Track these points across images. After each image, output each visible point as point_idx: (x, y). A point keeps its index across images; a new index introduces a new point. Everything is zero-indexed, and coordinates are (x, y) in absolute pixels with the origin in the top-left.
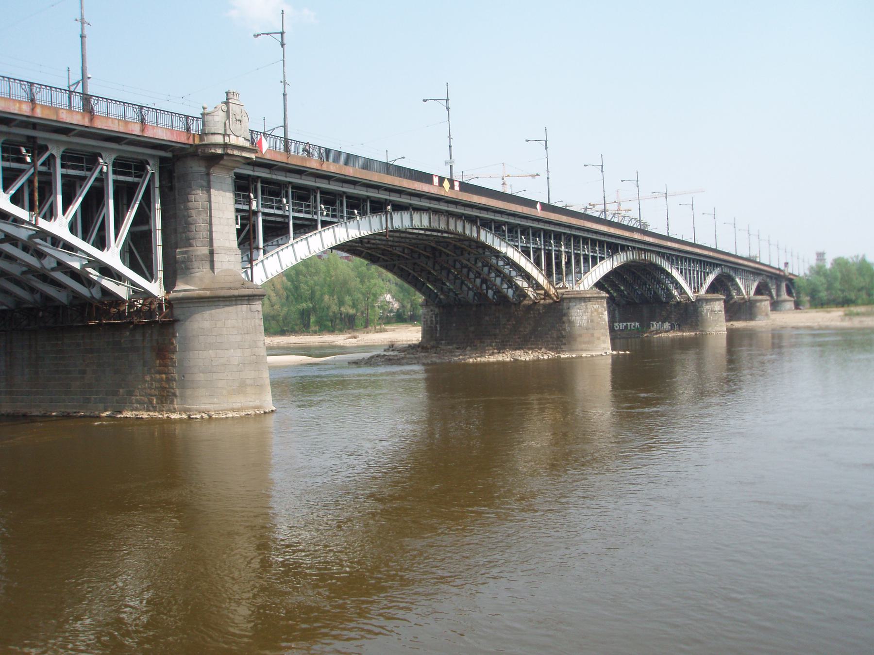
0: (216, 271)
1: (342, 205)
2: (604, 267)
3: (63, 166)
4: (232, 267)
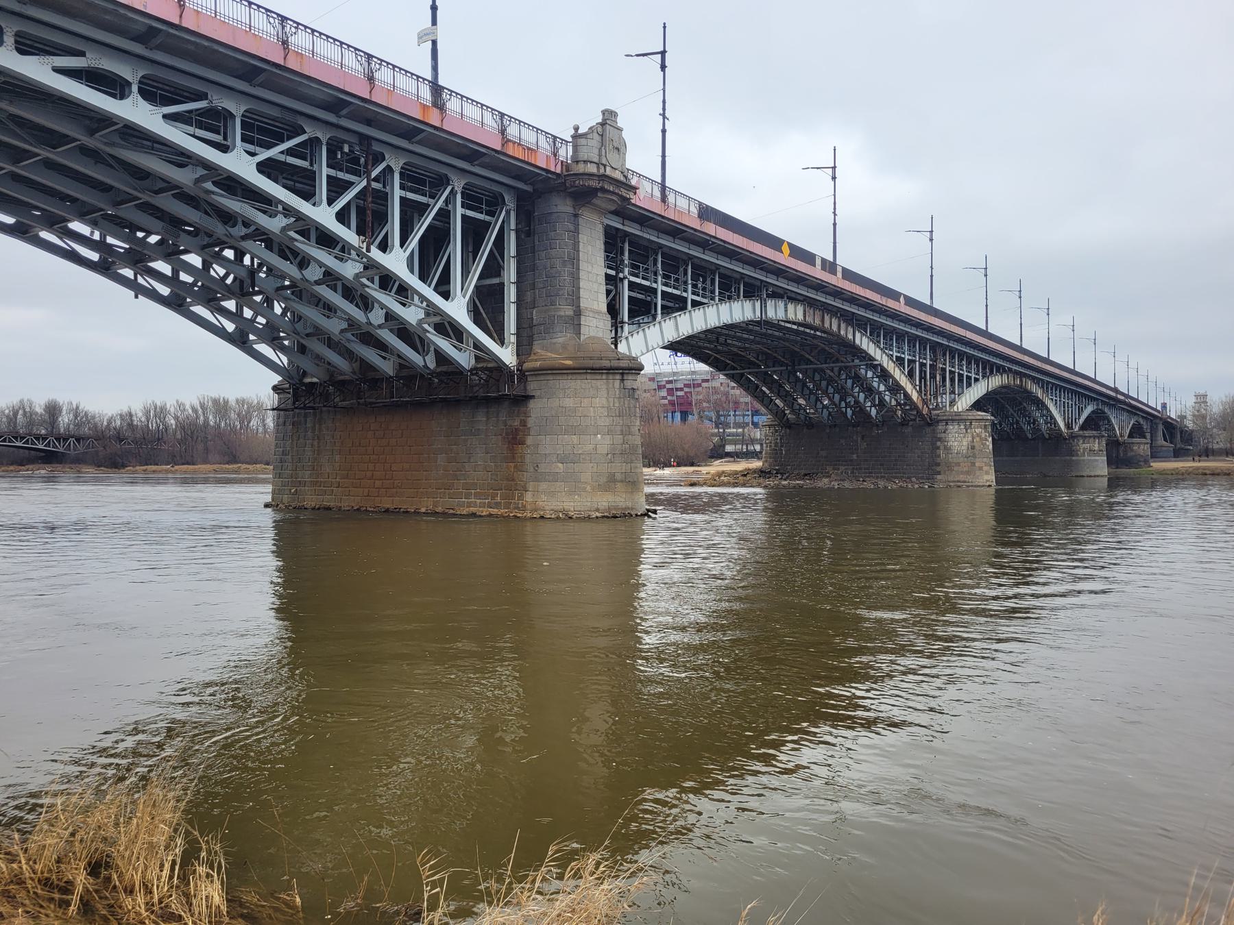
0: (582, 338)
2: (978, 390)
3: (402, 187)
4: (600, 335)
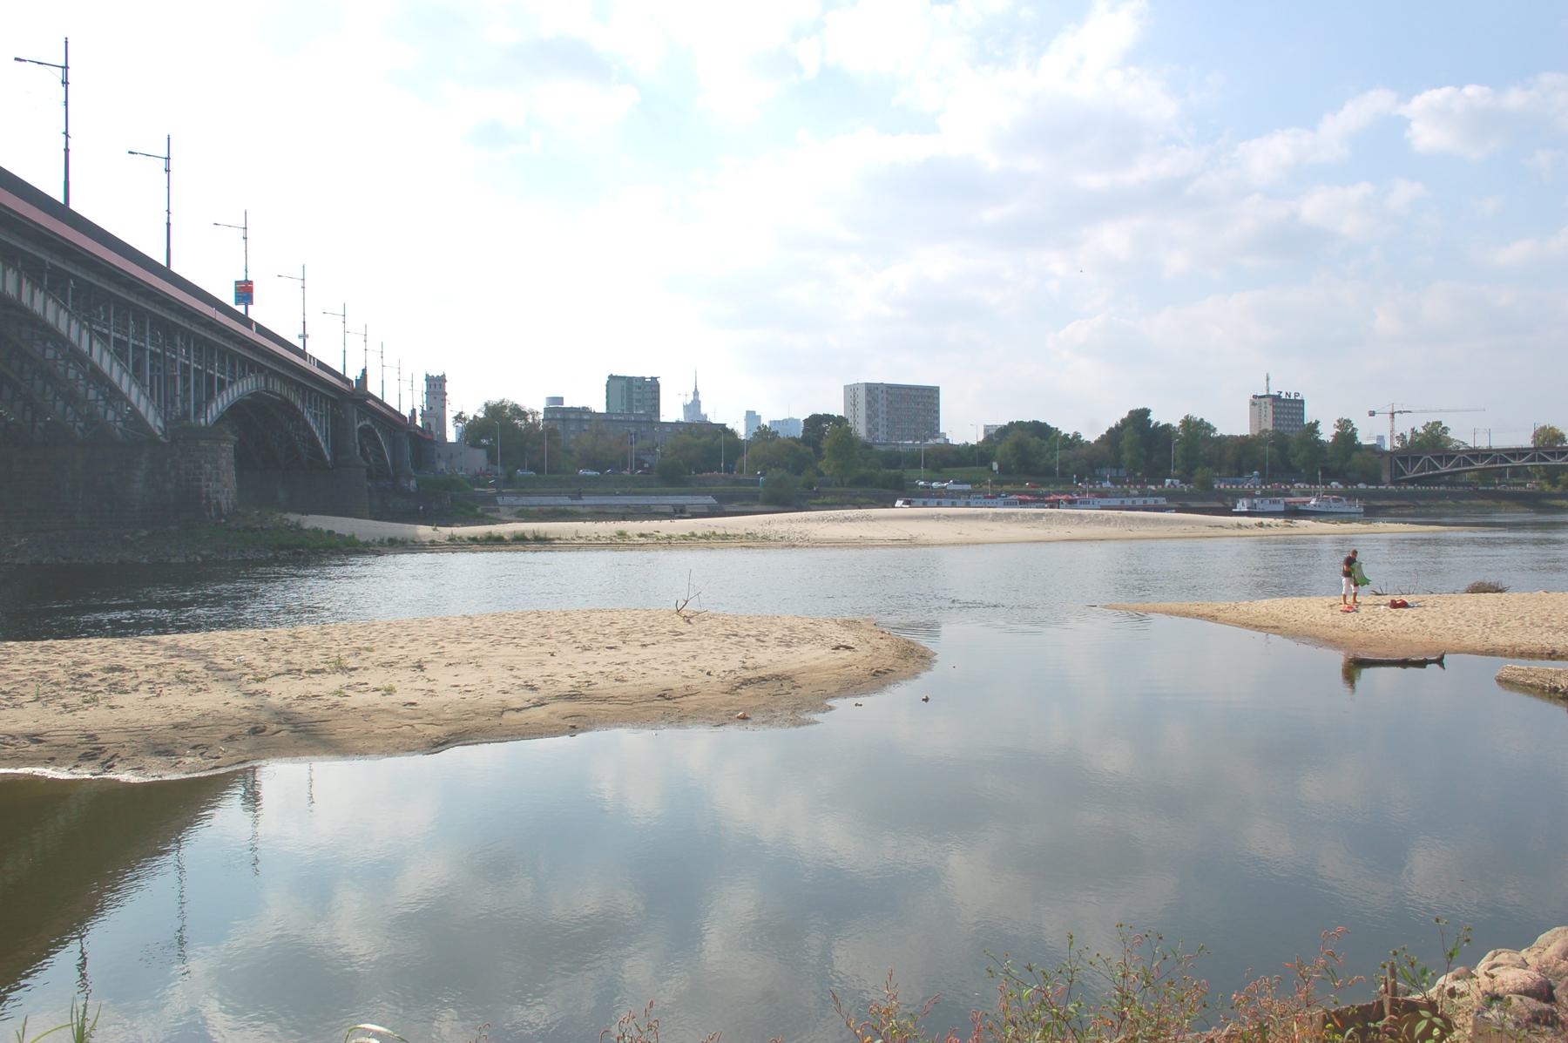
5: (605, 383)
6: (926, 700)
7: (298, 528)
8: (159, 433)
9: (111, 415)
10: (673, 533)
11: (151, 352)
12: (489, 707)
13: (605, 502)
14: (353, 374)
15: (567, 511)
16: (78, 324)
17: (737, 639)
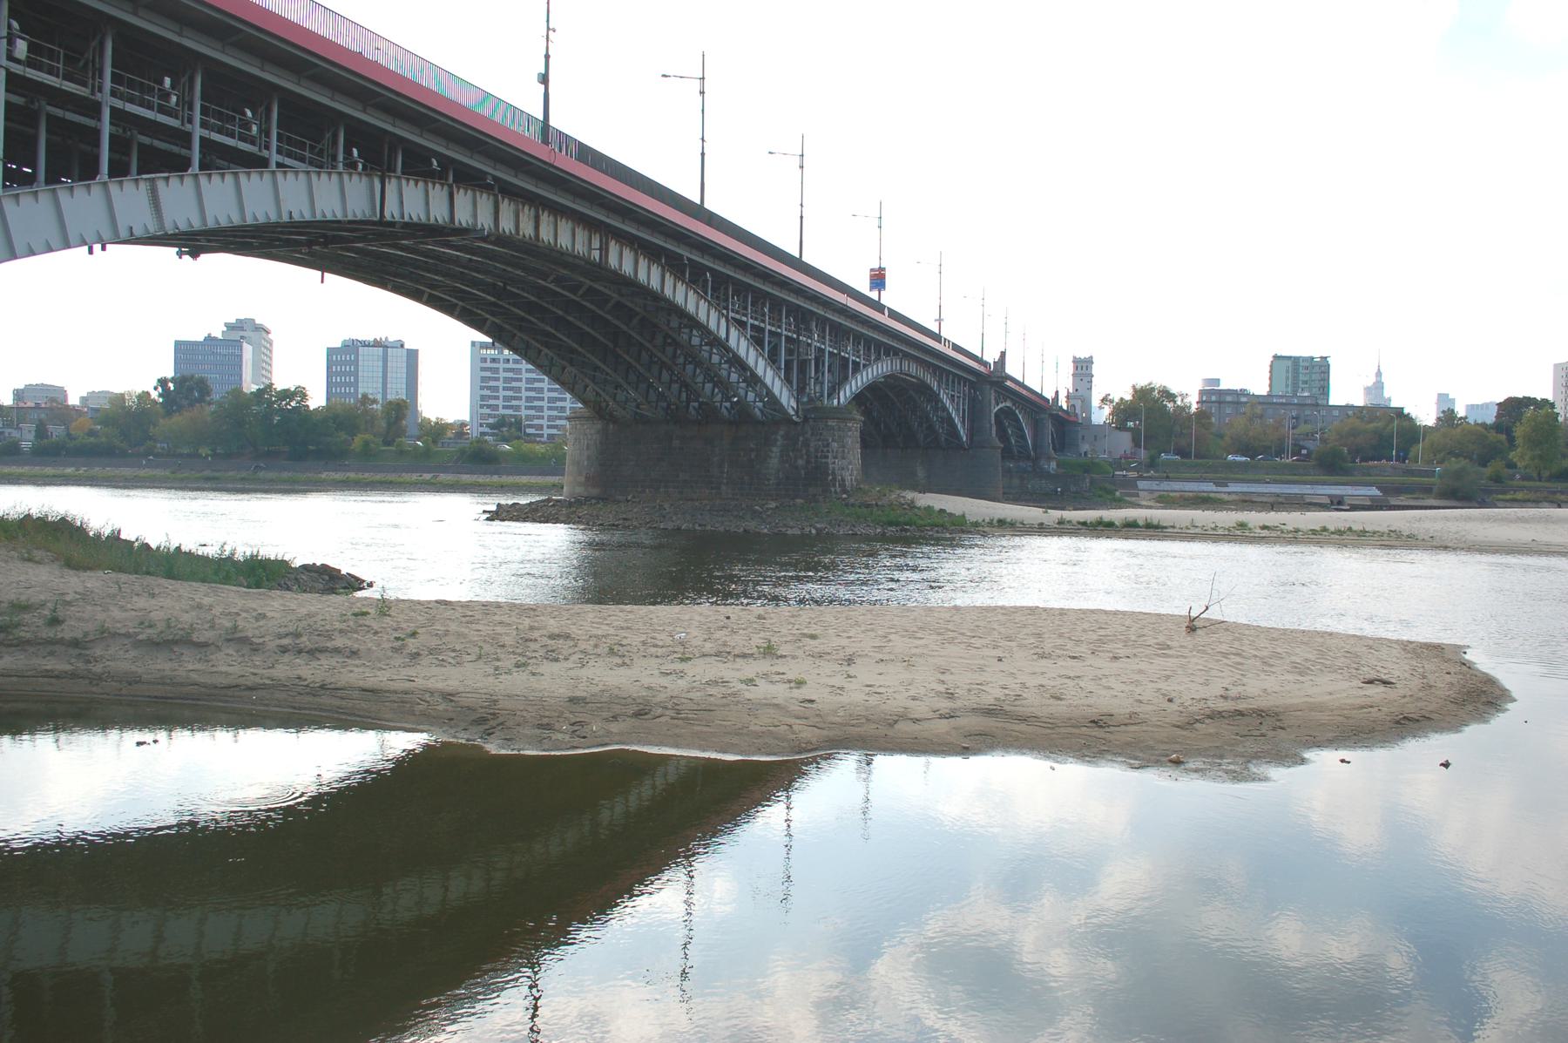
1: (335, 143)
5: (1269, 363)
6: (1446, 765)
7: (912, 505)
8: (793, 413)
9: (751, 396)
10: (1301, 527)
11: (787, 337)
12: (886, 714)
13: (1253, 490)
14: (991, 357)
15: (1210, 498)
16: (717, 313)
17: (1238, 659)
